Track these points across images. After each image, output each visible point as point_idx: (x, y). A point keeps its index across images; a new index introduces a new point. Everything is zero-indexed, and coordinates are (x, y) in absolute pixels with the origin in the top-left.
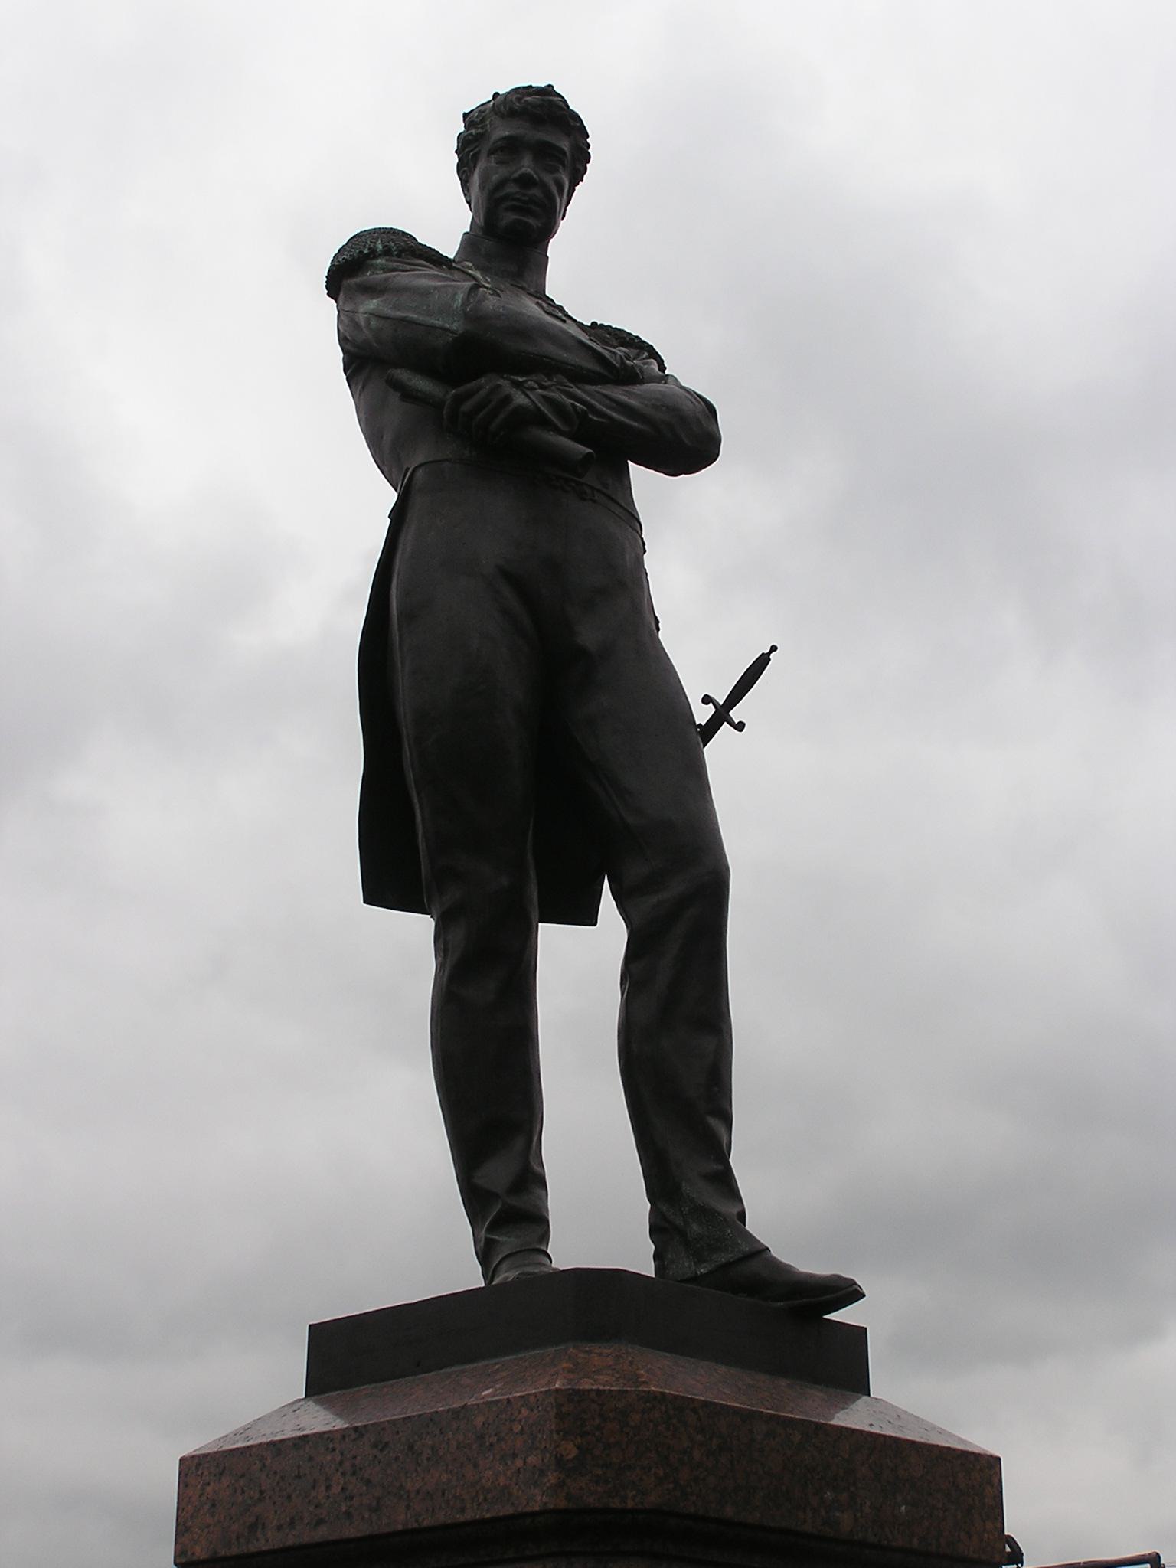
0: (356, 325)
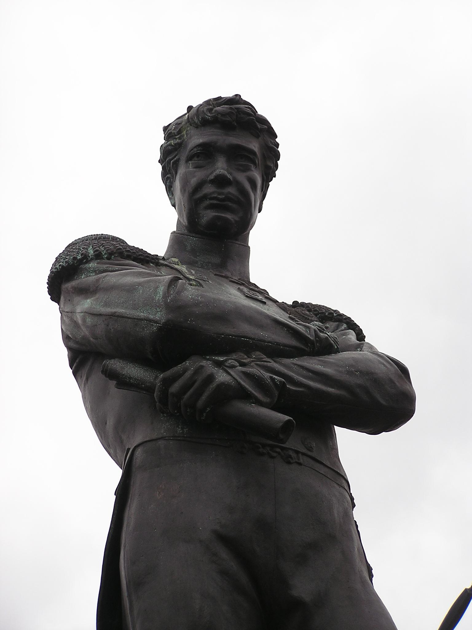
0: (75, 324)
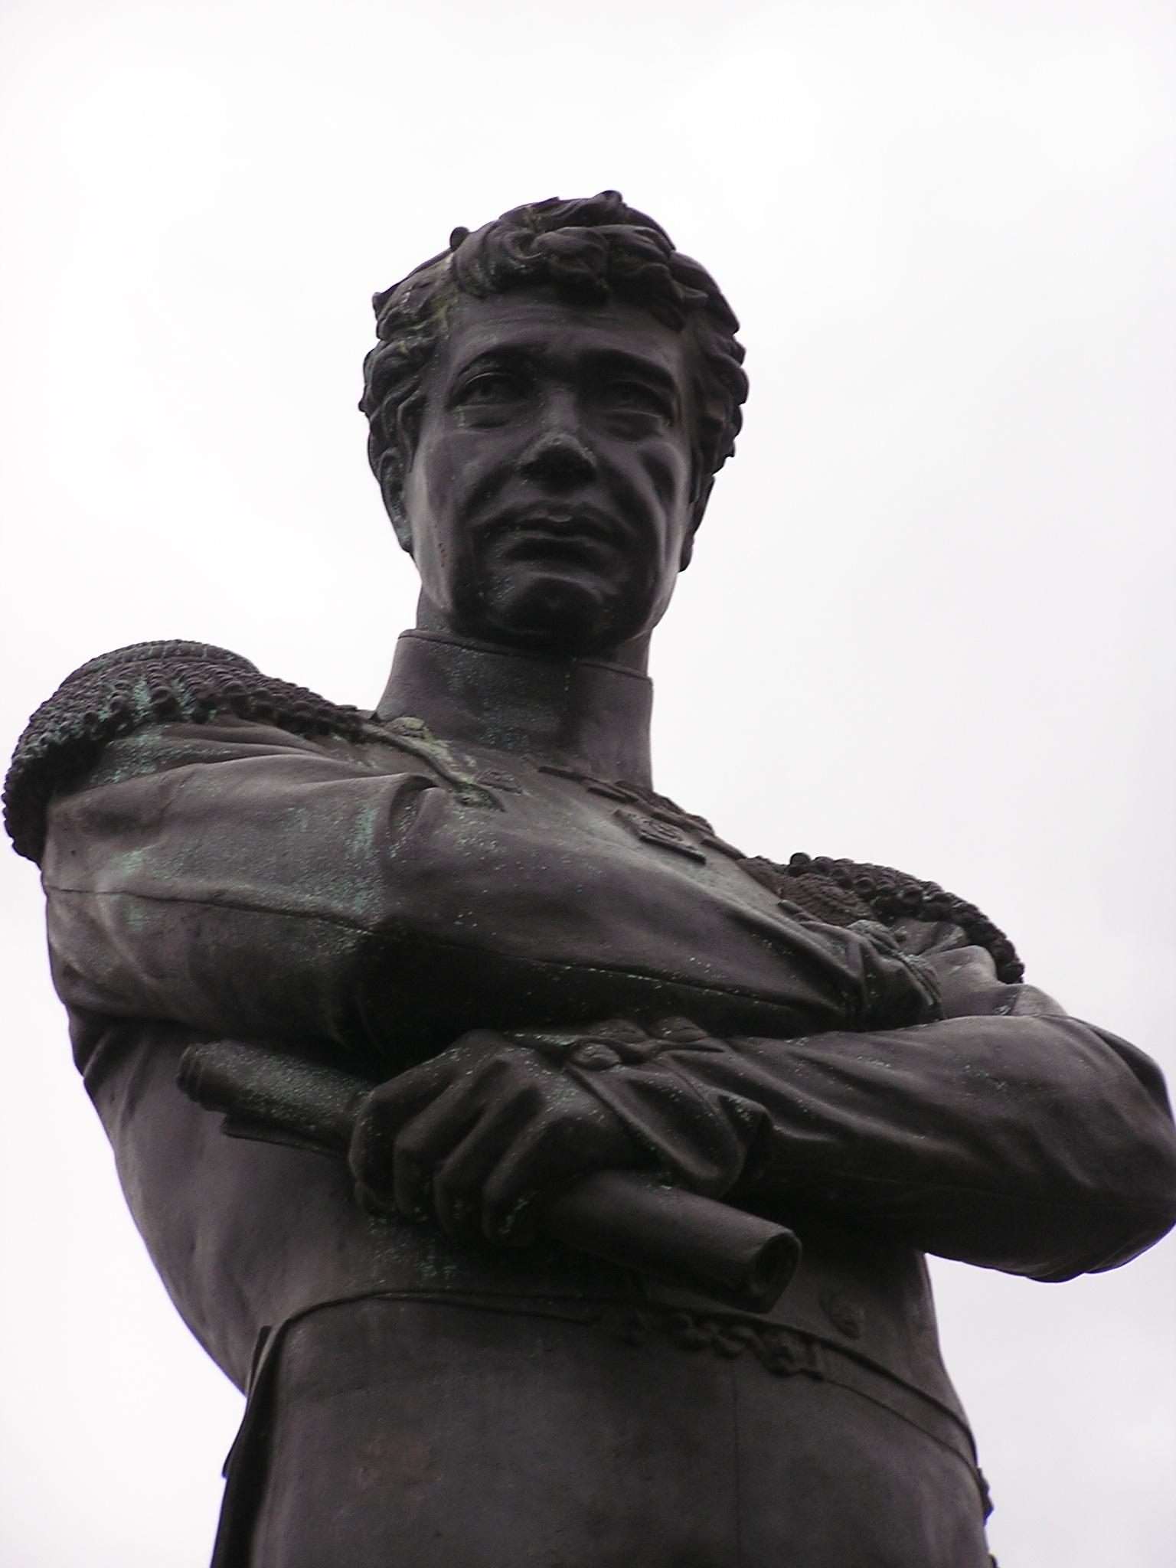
0: (93, 929)
